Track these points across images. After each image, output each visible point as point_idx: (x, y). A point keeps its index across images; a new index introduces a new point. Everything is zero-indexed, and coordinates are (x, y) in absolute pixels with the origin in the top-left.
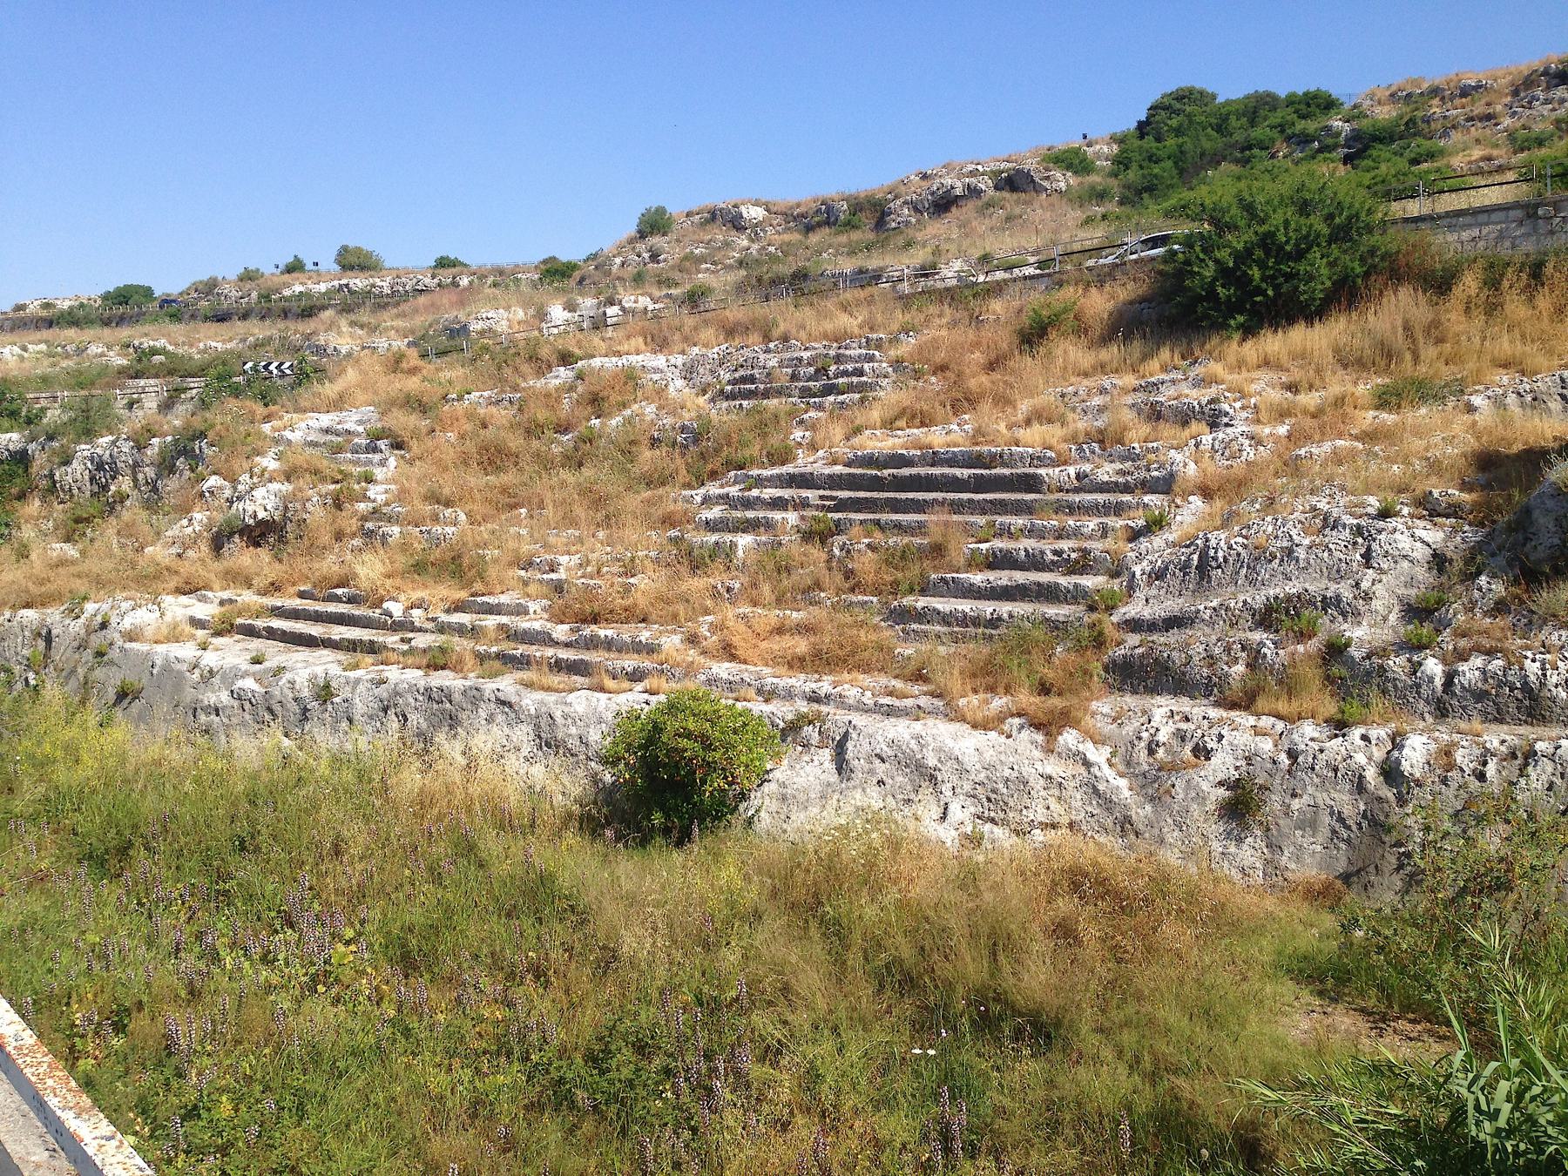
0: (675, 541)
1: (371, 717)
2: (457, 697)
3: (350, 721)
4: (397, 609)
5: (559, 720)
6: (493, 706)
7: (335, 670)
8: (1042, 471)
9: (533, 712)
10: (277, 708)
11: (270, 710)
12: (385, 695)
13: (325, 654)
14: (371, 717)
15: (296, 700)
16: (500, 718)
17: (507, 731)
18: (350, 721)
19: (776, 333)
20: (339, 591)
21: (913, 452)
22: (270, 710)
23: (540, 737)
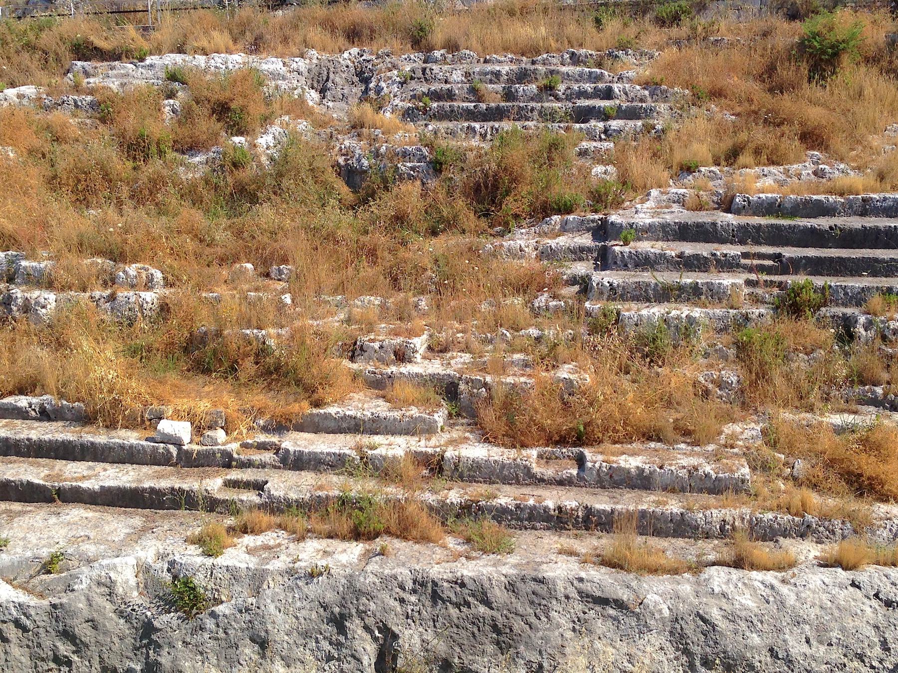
0: (317, 404)
1: (306, 635)
2: (499, 595)
3: (263, 644)
4: (178, 428)
5: (722, 625)
6: (579, 607)
7: (191, 557)
8: (80, 484)
9: (666, 613)
10: (83, 631)
11: (68, 635)
12: (330, 597)
13: (76, 513)
14: (306, 635)
15: (121, 614)
16: (601, 626)
17: (624, 648)
18: (263, 644)
19: (438, 36)
20: (22, 401)
21: (832, 198)
22: (68, 635)
23: (686, 652)
